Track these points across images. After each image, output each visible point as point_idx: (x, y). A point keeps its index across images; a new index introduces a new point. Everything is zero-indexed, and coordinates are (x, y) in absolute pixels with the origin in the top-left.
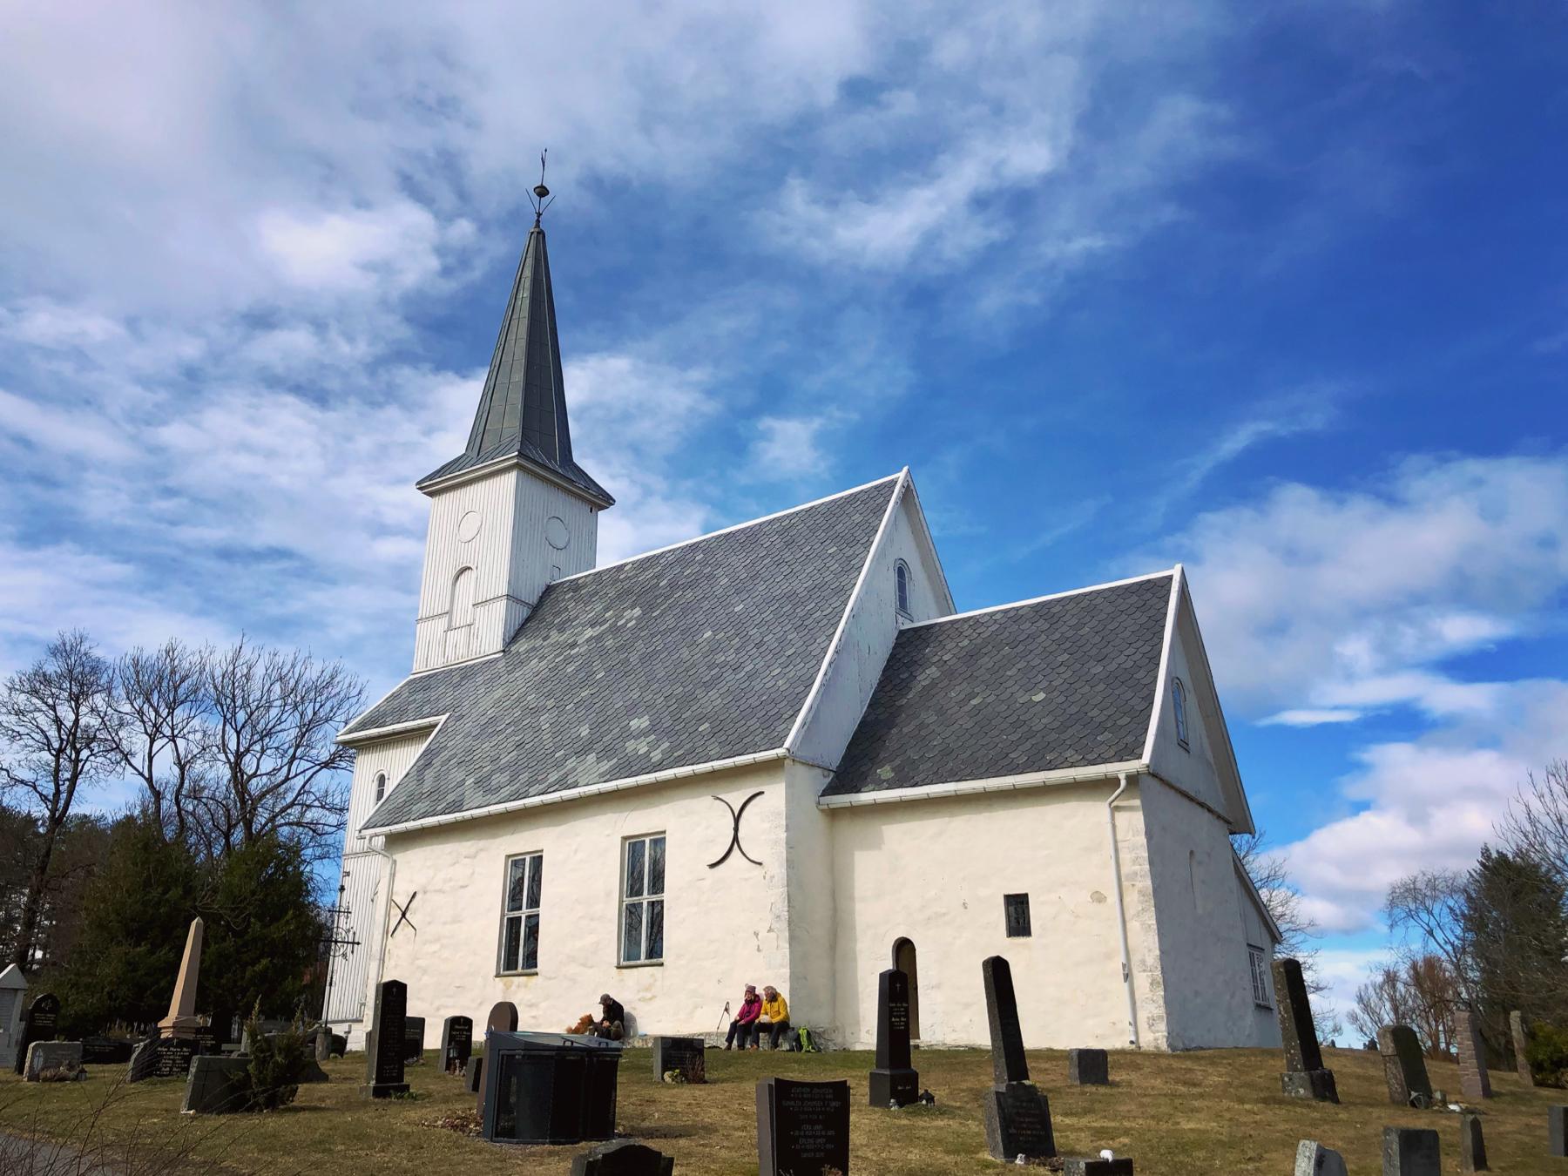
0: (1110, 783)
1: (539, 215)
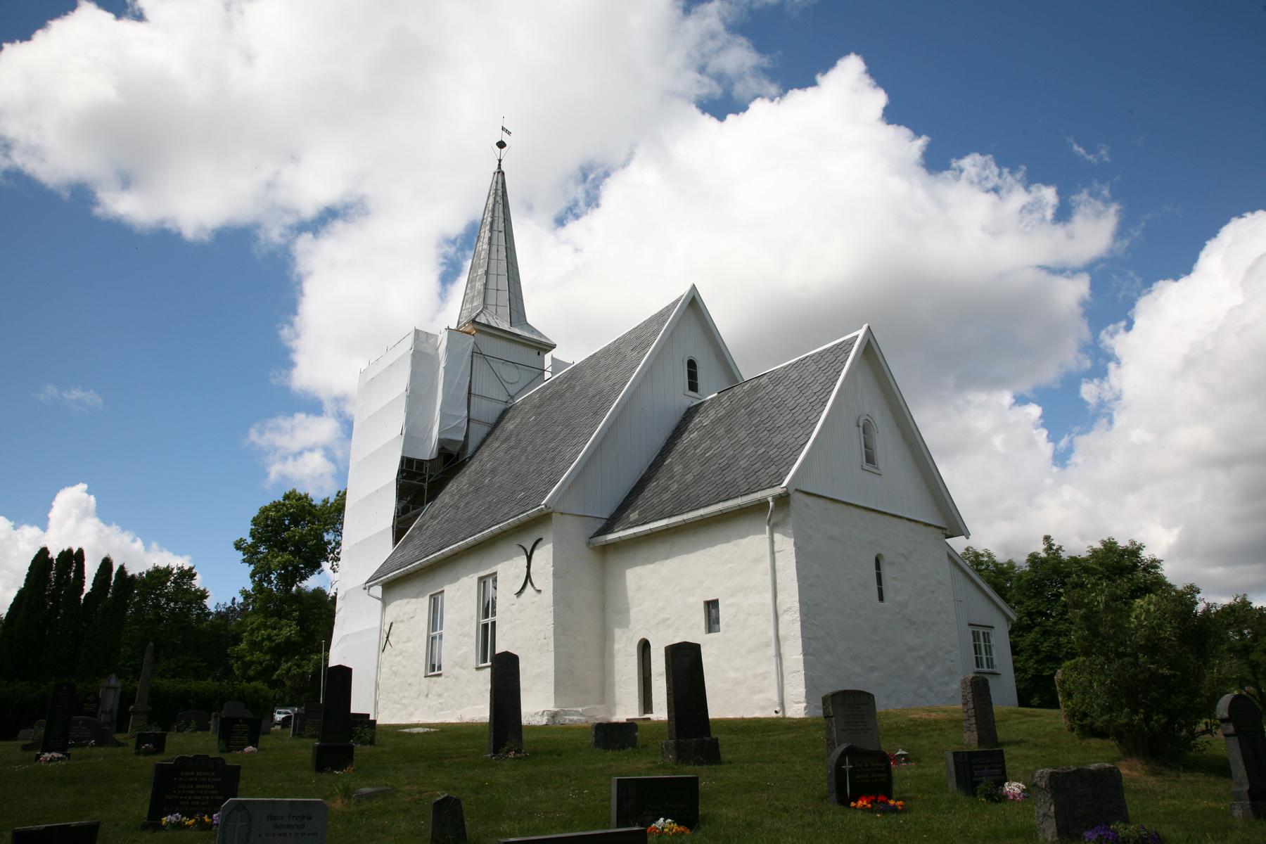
0: (761, 506)
1: (500, 161)
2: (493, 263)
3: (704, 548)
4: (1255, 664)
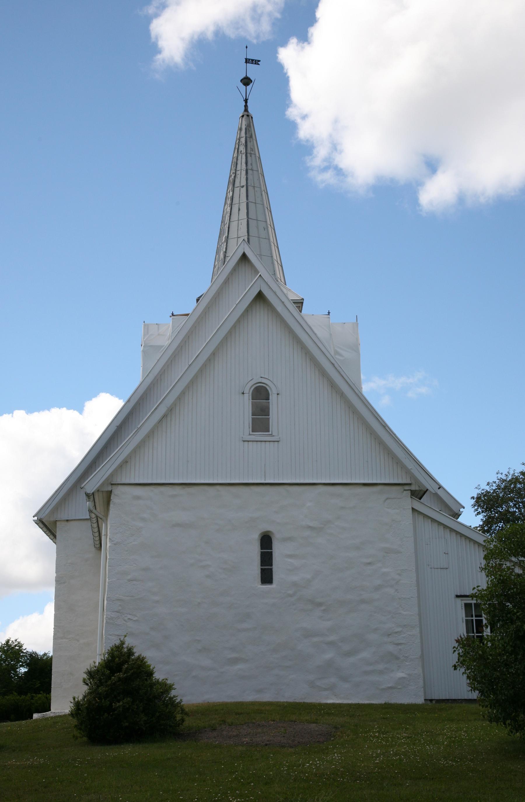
1: (246, 101)
2: (234, 225)
3: (82, 474)
4: (107, 619)
